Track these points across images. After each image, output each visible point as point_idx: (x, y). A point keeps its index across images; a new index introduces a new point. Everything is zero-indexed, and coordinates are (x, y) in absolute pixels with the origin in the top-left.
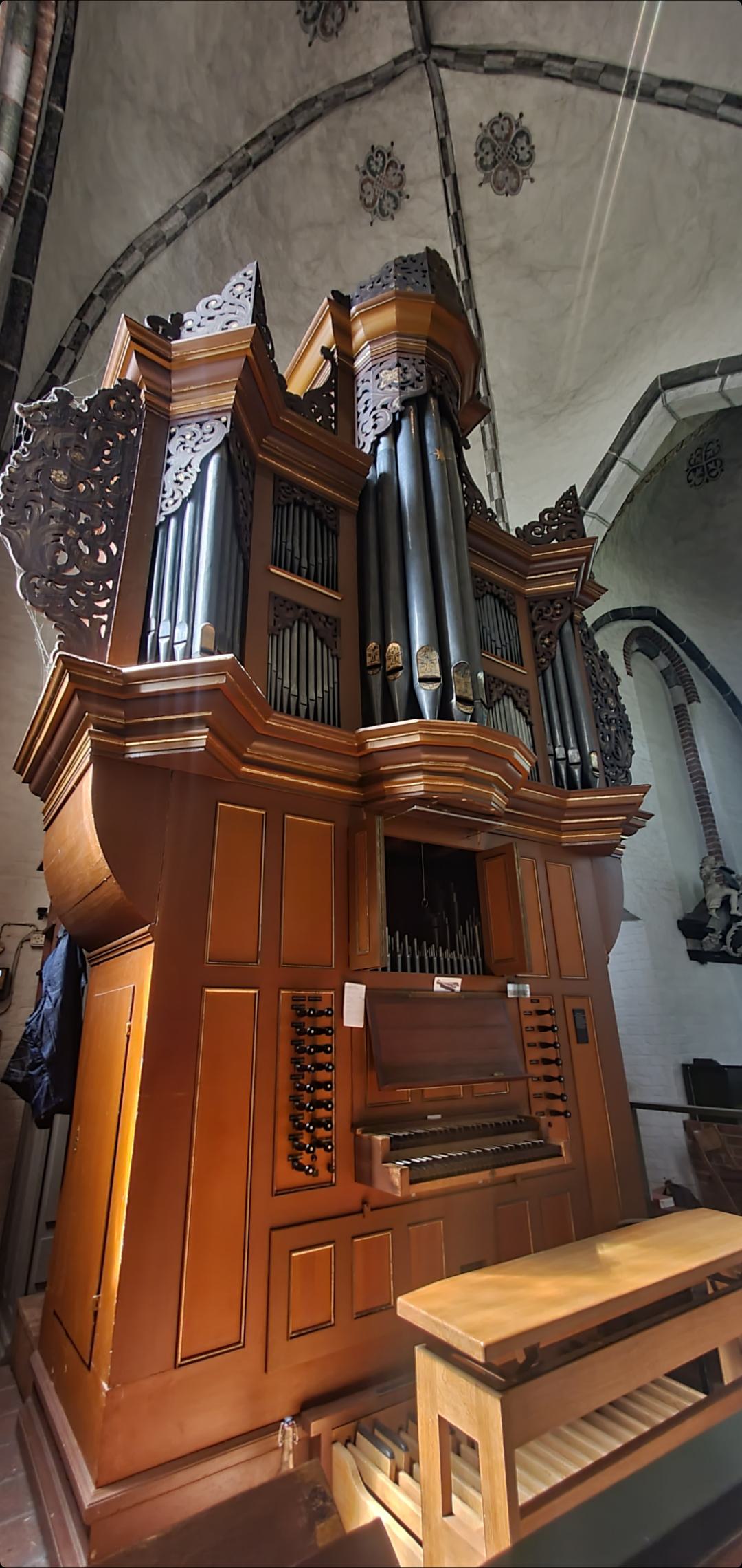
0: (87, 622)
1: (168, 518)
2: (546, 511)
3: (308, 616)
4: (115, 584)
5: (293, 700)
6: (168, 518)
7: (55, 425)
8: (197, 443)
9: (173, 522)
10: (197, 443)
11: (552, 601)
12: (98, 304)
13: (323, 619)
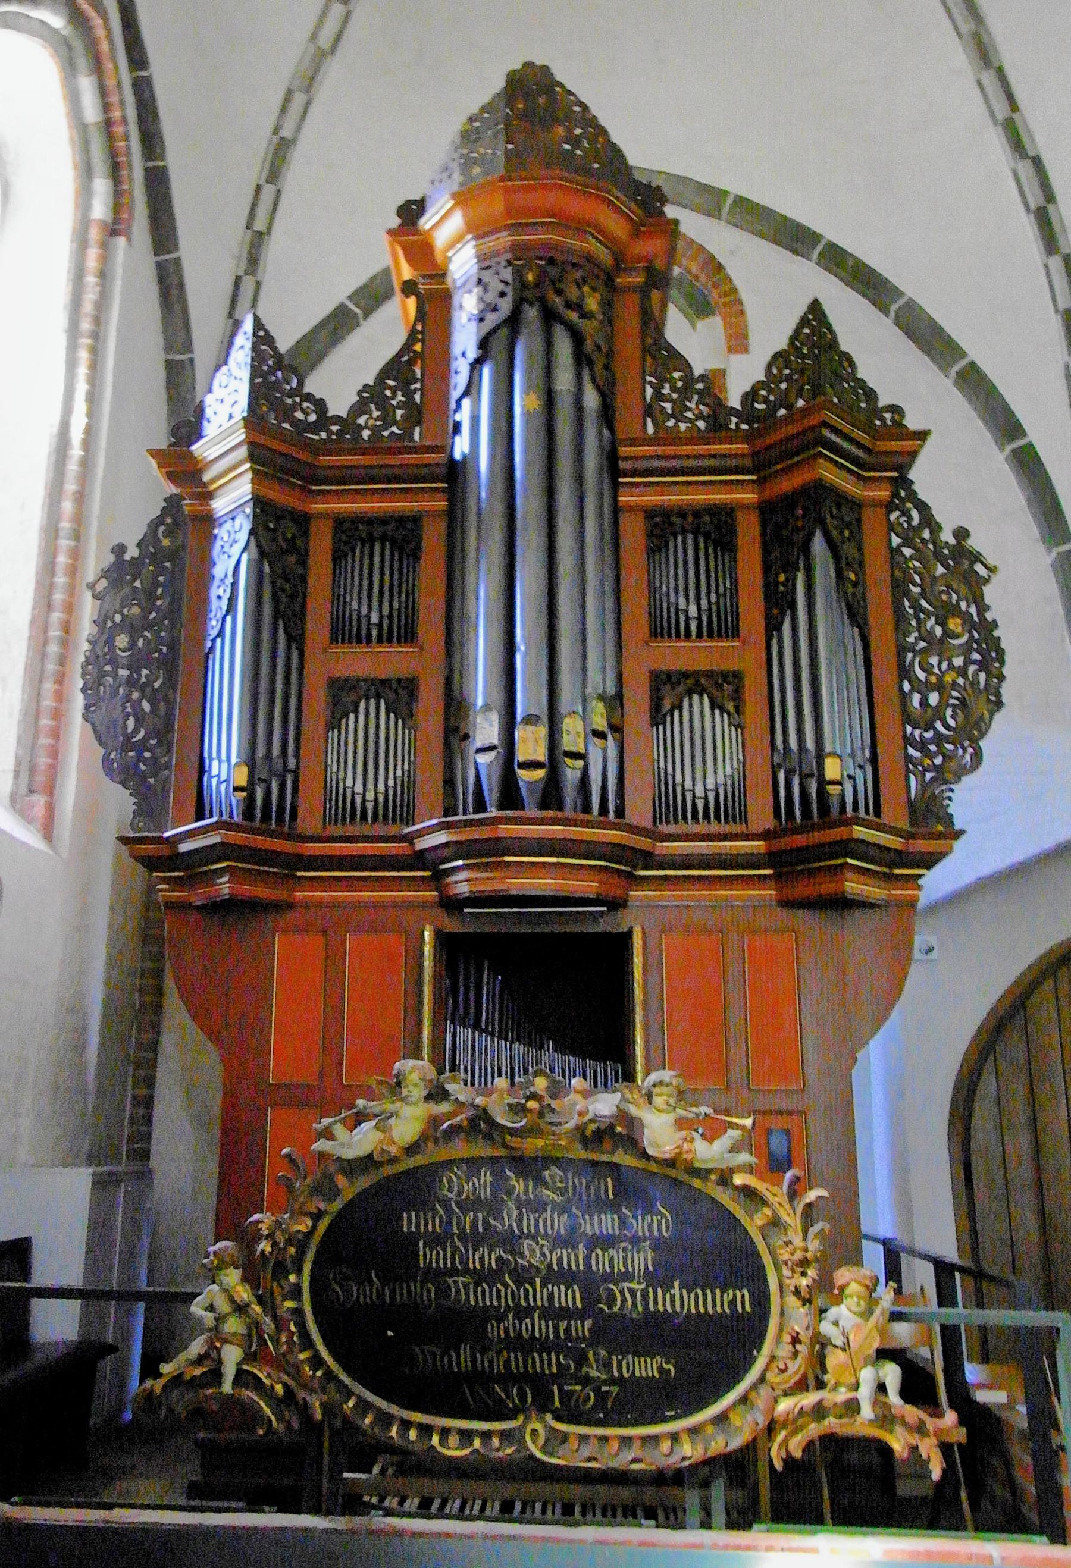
3: (379, 688)
12: (268, 191)
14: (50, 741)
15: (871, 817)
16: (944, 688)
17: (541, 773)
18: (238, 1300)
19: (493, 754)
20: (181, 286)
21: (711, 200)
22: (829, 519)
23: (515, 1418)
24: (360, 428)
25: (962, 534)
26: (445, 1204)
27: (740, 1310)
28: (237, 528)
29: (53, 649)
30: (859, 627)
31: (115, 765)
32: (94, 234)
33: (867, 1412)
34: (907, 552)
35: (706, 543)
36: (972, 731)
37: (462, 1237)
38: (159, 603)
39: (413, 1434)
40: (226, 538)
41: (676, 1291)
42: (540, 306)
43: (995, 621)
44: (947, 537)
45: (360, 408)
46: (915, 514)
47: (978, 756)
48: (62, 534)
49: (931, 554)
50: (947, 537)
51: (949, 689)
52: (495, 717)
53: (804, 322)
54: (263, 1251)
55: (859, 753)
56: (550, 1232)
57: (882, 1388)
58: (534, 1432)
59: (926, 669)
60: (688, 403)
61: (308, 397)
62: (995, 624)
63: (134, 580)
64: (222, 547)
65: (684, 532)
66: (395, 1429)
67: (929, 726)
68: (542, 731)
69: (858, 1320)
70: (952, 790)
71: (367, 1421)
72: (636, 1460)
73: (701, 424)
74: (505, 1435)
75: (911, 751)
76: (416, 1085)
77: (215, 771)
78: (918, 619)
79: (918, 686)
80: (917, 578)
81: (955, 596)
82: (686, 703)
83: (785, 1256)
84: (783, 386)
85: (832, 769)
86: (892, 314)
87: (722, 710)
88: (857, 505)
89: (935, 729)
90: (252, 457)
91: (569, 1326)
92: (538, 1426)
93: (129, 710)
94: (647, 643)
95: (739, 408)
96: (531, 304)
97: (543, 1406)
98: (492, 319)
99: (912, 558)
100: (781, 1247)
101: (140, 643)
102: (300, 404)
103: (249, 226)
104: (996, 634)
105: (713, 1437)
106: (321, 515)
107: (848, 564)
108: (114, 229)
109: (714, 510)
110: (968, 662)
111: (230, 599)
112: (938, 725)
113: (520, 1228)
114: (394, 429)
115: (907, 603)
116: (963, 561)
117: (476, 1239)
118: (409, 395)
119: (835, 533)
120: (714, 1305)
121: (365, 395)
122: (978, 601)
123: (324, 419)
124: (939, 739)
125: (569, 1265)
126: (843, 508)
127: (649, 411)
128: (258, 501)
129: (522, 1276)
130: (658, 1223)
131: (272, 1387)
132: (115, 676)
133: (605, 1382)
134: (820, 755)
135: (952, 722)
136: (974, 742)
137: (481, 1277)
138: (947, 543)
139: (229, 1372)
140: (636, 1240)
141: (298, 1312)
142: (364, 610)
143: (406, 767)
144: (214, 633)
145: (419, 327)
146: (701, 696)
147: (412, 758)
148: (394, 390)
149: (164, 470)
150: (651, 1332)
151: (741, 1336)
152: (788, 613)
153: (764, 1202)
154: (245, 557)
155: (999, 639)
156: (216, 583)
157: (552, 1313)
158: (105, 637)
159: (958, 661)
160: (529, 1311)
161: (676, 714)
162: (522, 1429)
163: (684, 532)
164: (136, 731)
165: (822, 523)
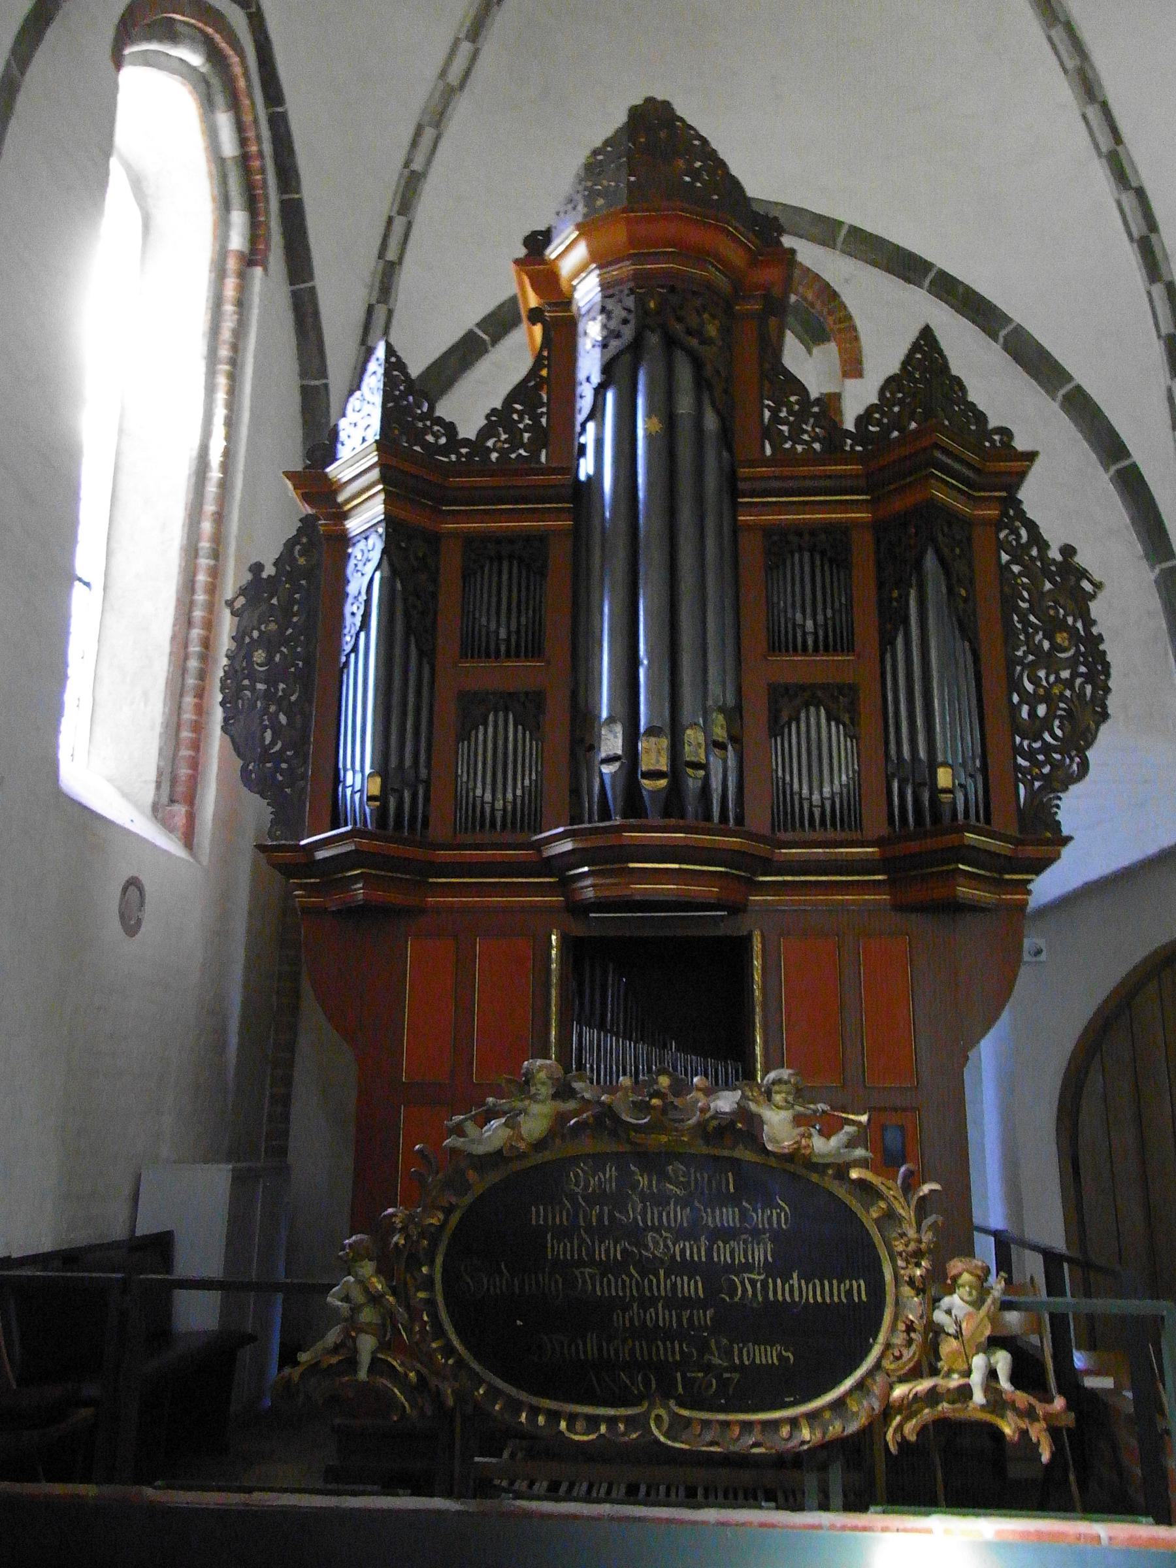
3: (507, 701)
5: (488, 809)
15: (982, 824)
19: (617, 765)
22: (940, 537)
26: (572, 1197)
33: (979, 1397)
34: (1016, 569)
36: (1080, 738)
37: (589, 1229)
38: (295, 619)
40: (359, 557)
44: (1054, 554)
45: (487, 431)
47: (1084, 767)
50: (1054, 554)
52: (618, 729)
55: (970, 763)
57: (992, 1374)
58: (658, 1418)
59: (1035, 680)
61: (439, 421)
62: (1100, 638)
64: (356, 565)
66: (524, 1415)
67: (1038, 737)
70: (1060, 799)
71: (497, 1407)
73: (817, 446)
74: (628, 1420)
75: (1020, 761)
76: (543, 1084)
77: (349, 782)
79: (1026, 698)
80: (1025, 594)
81: (1061, 611)
82: (803, 715)
83: (900, 1248)
85: (944, 778)
88: (968, 523)
89: (1044, 740)
91: (692, 1315)
92: (662, 1412)
95: (853, 430)
97: (667, 1392)
98: (615, 344)
99: (1021, 574)
100: (896, 1239)
101: (277, 658)
102: (431, 427)
104: (1101, 647)
105: (830, 1422)
107: (959, 580)
109: (829, 528)
110: (1075, 675)
111: (363, 616)
112: (1047, 736)
113: (644, 1220)
114: (522, 451)
115: (1016, 618)
116: (1070, 582)
117: (601, 1232)
118: (536, 418)
119: (946, 551)
121: (494, 418)
123: (454, 442)
124: (1047, 749)
127: (768, 433)
129: (647, 1268)
131: (406, 1375)
132: (253, 689)
133: (726, 1370)
134: (933, 766)
135: (1059, 733)
137: (607, 1268)
139: (365, 1359)
140: (756, 1233)
141: (431, 1303)
144: (348, 648)
148: (521, 414)
150: (772, 1320)
151: (860, 1323)
153: (880, 1196)
154: (378, 575)
157: (675, 1302)
158: (243, 652)
159: (1065, 674)
160: (653, 1301)
164: (273, 743)
165: (933, 540)
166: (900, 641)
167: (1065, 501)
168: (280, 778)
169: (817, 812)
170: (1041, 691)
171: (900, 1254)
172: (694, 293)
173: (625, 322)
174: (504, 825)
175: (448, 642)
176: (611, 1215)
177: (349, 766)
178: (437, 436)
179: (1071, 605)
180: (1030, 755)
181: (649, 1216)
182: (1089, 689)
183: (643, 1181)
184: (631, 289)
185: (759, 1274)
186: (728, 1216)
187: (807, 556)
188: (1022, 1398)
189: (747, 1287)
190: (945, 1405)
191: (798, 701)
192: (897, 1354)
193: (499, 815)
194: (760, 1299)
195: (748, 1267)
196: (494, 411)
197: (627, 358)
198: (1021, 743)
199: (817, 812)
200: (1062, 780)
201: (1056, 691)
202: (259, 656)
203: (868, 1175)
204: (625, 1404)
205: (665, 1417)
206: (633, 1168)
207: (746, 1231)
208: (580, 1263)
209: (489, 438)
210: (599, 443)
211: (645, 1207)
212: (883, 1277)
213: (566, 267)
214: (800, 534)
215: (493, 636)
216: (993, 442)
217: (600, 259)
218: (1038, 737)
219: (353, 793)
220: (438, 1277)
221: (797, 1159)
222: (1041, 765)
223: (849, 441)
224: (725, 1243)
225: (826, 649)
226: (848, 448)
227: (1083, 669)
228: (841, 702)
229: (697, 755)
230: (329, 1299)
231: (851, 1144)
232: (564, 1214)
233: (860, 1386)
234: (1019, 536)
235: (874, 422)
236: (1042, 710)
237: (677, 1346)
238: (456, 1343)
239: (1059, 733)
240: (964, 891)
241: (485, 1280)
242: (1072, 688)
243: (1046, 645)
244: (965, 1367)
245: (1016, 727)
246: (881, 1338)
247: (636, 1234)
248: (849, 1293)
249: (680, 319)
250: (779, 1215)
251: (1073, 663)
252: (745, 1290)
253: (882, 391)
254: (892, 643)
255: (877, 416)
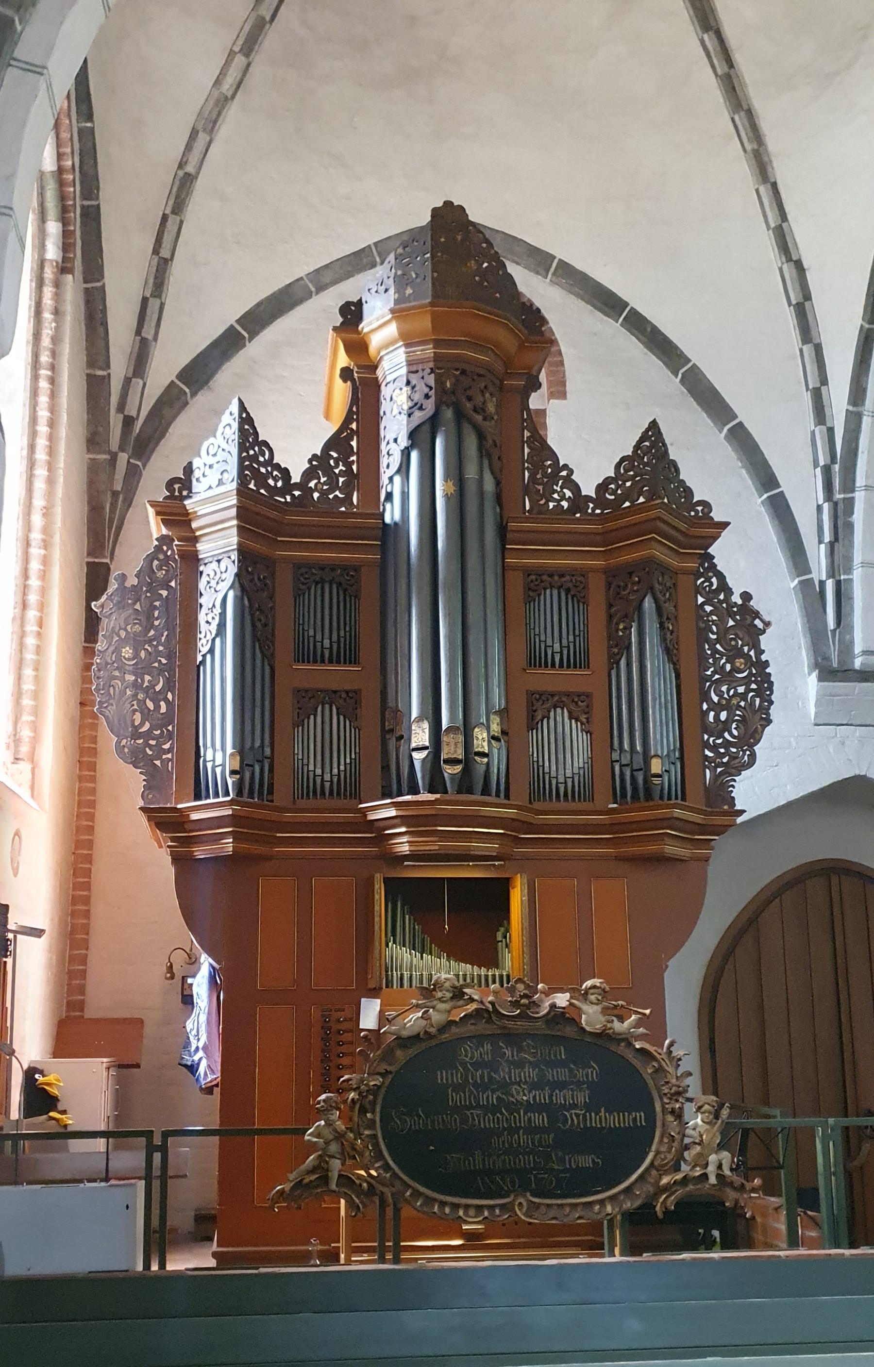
0: (158, 763)
1: (204, 656)
2: (623, 459)
3: (331, 696)
4: (173, 727)
5: (318, 780)
6: (204, 656)
7: (119, 609)
8: (218, 583)
9: (208, 657)
10: (218, 583)
11: (631, 574)
12: (172, 221)
13: (344, 695)
14: (32, 718)
15: (679, 801)
16: (731, 707)
17: (458, 768)
18: (339, 1130)
19: (426, 752)
20: (104, 311)
21: (540, 260)
22: (657, 586)
23: (508, 1196)
24: (311, 491)
25: (746, 596)
26: (464, 1064)
27: (639, 1124)
28: (223, 569)
29: (31, 641)
30: (674, 664)
31: (126, 750)
32: (49, 274)
33: (713, 1180)
34: (708, 608)
35: (567, 595)
36: (751, 737)
37: (475, 1084)
38: (156, 623)
39: (447, 1210)
40: (212, 575)
41: (602, 1114)
42: (454, 408)
43: (767, 661)
44: (736, 599)
45: (309, 474)
46: (714, 580)
47: (753, 757)
48: (33, 543)
49: (725, 612)
50: (736, 599)
51: (734, 708)
52: (426, 725)
53: (644, 437)
54: (353, 1099)
55: (672, 754)
56: (528, 1079)
57: (720, 1167)
58: (520, 1204)
59: (720, 694)
60: (555, 487)
61: (277, 467)
62: (766, 664)
63: (135, 603)
64: (209, 582)
65: (552, 587)
66: (436, 1207)
67: (721, 736)
68: (461, 738)
69: (707, 1127)
70: (735, 781)
71: (418, 1204)
72: (580, 1218)
73: (565, 504)
74: (502, 1207)
75: (707, 752)
76: (448, 991)
77: (209, 757)
78: (715, 659)
79: (713, 707)
80: (714, 628)
81: (740, 642)
82: (552, 714)
83: (666, 1091)
84: (628, 484)
85: (656, 766)
86: (680, 376)
87: (577, 720)
88: (675, 573)
89: (724, 738)
90: (239, 516)
91: (541, 1138)
92: (522, 1200)
93: (135, 707)
94: (524, 670)
95: (594, 496)
96: (448, 406)
97: (525, 1187)
98: (419, 416)
99: (711, 613)
100: (663, 1085)
101: (143, 654)
102: (272, 473)
103: (156, 251)
104: (767, 671)
105: (624, 1201)
106: (285, 559)
107: (668, 618)
108: (64, 268)
109: (573, 572)
110: (749, 690)
111: (219, 625)
112: (726, 735)
113: (510, 1078)
114: (337, 493)
115: (707, 647)
116: (748, 620)
117: (482, 1087)
118: (349, 465)
119: (659, 595)
120: (624, 1123)
121: (314, 463)
122: (756, 645)
123: (289, 486)
124: (727, 744)
125: (540, 1100)
126: (666, 576)
127: (527, 490)
128: (242, 550)
129: (513, 1107)
130: (592, 1072)
131: (361, 1185)
132: (123, 680)
133: (562, 1171)
134: (647, 758)
135: (735, 733)
136: (751, 746)
137: (493, 1109)
138: (735, 603)
139: (334, 1175)
140: (579, 1084)
141: (375, 1136)
142: (319, 637)
143: (353, 756)
144: (204, 650)
145: (354, 409)
146: (562, 709)
147: (357, 751)
148: (337, 461)
149: (159, 518)
150: (588, 1139)
151: (637, 1141)
152: (625, 652)
153: (654, 1058)
154: (231, 594)
155: (770, 674)
156: (204, 611)
157: (531, 1130)
158: (112, 648)
159: (741, 690)
160: (517, 1130)
161: (545, 721)
162: (512, 1203)
163: (552, 587)
164: (142, 724)
165: (652, 588)
166: (623, 662)
167: (747, 561)
168: (150, 753)
169: (562, 788)
170: (724, 702)
171: (665, 1094)
172: (479, 375)
173: (427, 396)
174: (331, 793)
175: (284, 648)
176: (489, 1073)
177: (209, 744)
178: (276, 479)
179: (747, 639)
180: (714, 748)
181: (513, 1075)
182: (758, 700)
183: (508, 1053)
184: (432, 369)
185: (581, 1110)
186: (562, 1074)
187: (555, 592)
188: (737, 1180)
189: (573, 1118)
190: (692, 1187)
191: (548, 705)
192: (663, 1157)
193: (327, 785)
194: (582, 1126)
195: (575, 1106)
196: (314, 457)
197: (426, 428)
198: (708, 739)
199: (562, 788)
200: (737, 767)
201: (734, 702)
202: (127, 652)
203: (647, 1046)
204: (503, 1197)
205: (525, 1204)
206: (501, 1044)
207: (572, 1083)
208: (471, 1107)
209: (310, 481)
210: (405, 496)
211: (510, 1070)
212: (654, 1108)
213: (375, 341)
214: (551, 576)
215: (319, 645)
216: (697, 512)
217: (408, 339)
218: (721, 736)
219: (214, 768)
220: (378, 1119)
221: (604, 1035)
222: (723, 755)
223: (591, 505)
224: (560, 1091)
225: (575, 667)
226: (590, 511)
227: (754, 686)
228: (579, 705)
229: (483, 747)
230: (307, 1138)
231: (637, 1025)
232: (459, 1075)
233: (642, 1177)
234: (711, 584)
235: (610, 491)
236: (723, 716)
237: (531, 1158)
238: (391, 1163)
239: (735, 733)
240: (671, 849)
241: (408, 1120)
242: (745, 700)
243: (728, 667)
244: (705, 1162)
245: (706, 728)
246: (654, 1148)
247: (504, 1086)
248: (635, 1119)
249: (469, 399)
250: (592, 1073)
251: (747, 681)
252: (572, 1120)
253: (618, 466)
254: (618, 663)
255: (613, 486)
